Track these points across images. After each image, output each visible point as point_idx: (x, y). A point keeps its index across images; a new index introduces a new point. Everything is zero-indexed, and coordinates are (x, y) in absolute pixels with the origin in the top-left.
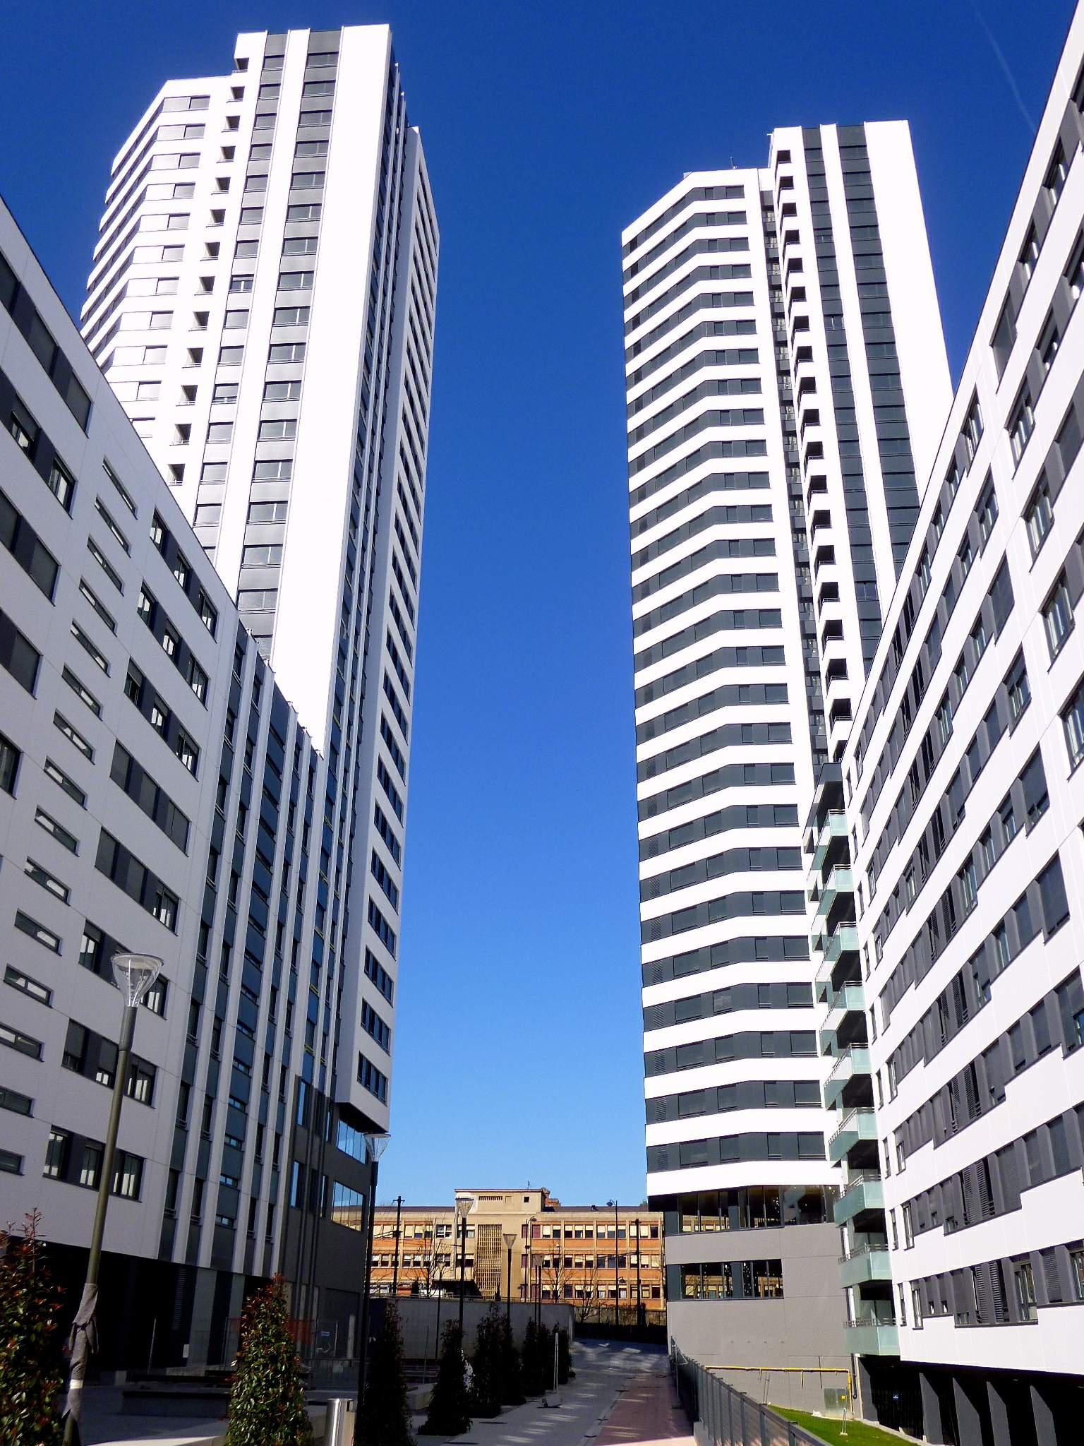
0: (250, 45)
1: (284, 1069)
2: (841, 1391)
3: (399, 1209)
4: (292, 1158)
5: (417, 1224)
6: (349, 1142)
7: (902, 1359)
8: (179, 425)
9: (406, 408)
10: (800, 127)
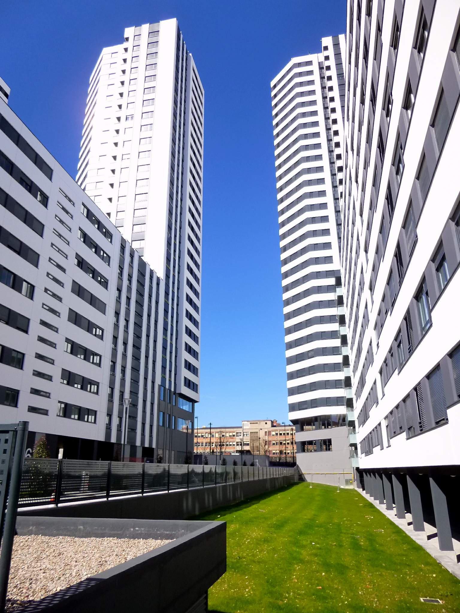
0: (129, 32)
1: (153, 382)
2: (351, 480)
3: (210, 428)
4: (159, 411)
5: (230, 432)
6: (186, 407)
7: (360, 468)
10: (331, 37)
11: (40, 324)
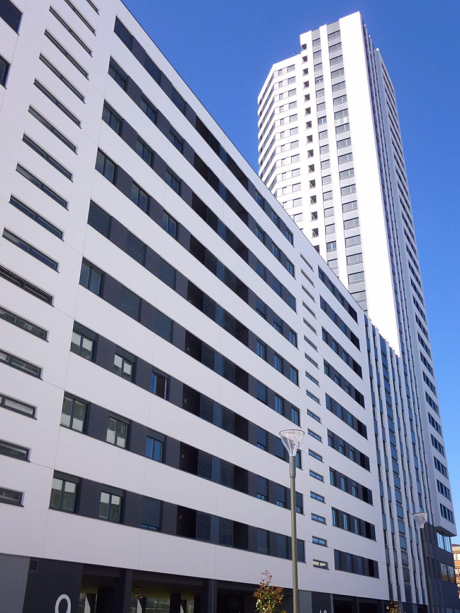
0: (306, 38)
8: (313, 229)
9: (391, 126)
11: (34, 84)
